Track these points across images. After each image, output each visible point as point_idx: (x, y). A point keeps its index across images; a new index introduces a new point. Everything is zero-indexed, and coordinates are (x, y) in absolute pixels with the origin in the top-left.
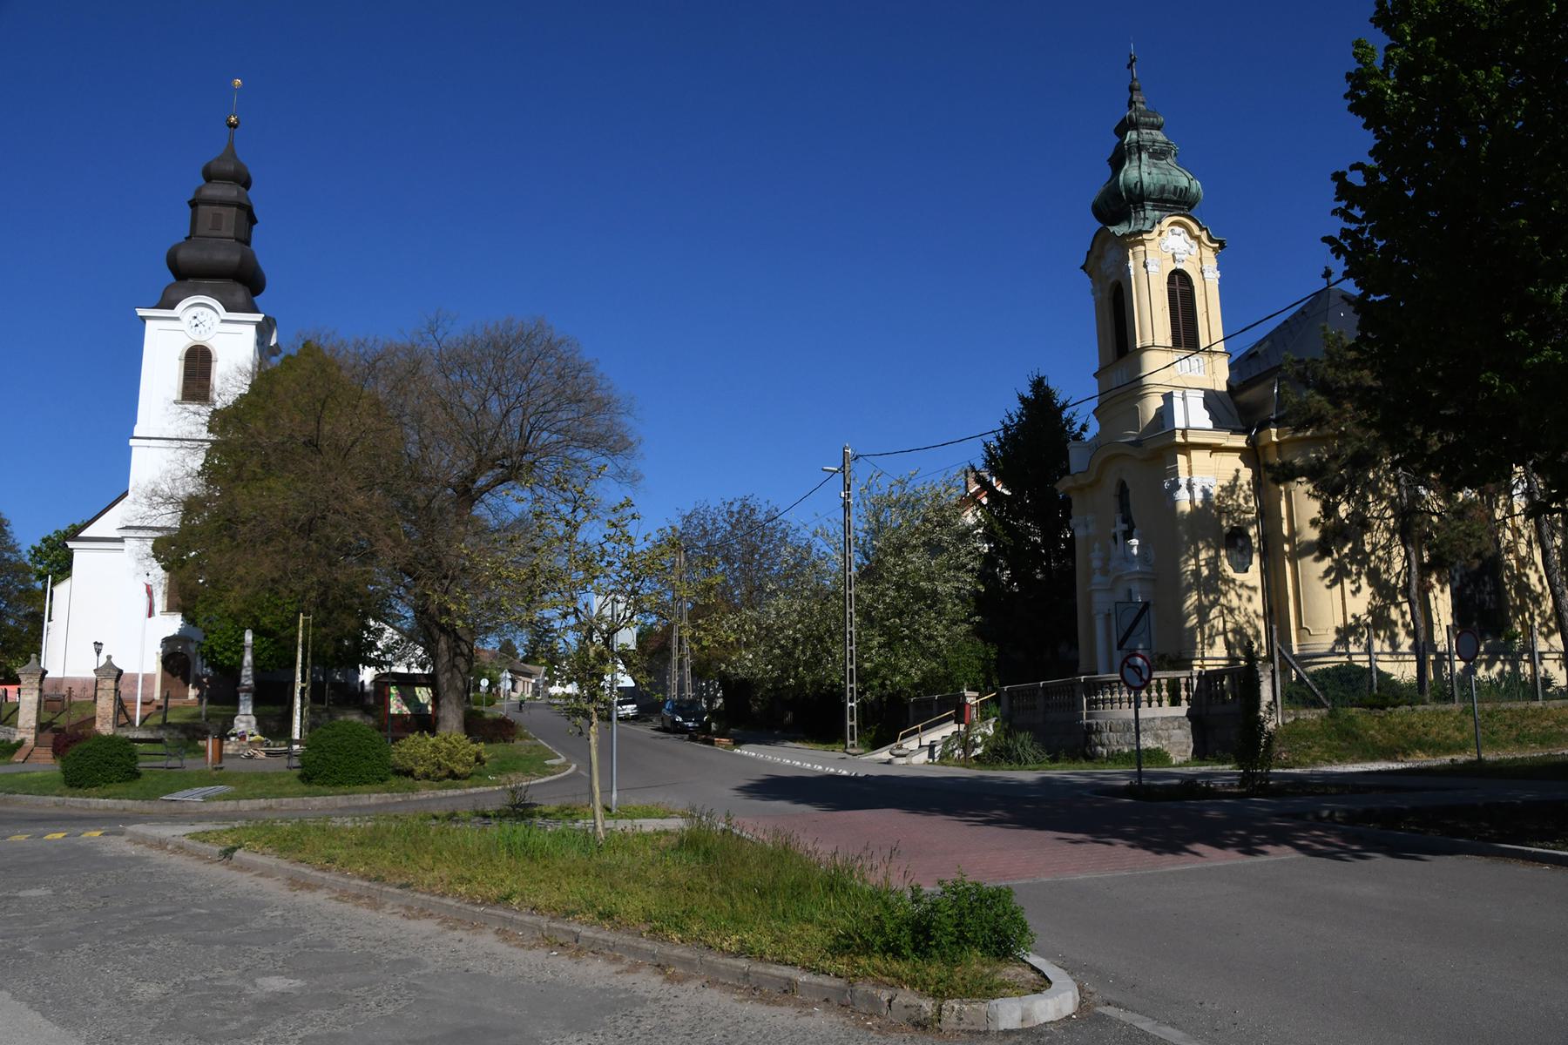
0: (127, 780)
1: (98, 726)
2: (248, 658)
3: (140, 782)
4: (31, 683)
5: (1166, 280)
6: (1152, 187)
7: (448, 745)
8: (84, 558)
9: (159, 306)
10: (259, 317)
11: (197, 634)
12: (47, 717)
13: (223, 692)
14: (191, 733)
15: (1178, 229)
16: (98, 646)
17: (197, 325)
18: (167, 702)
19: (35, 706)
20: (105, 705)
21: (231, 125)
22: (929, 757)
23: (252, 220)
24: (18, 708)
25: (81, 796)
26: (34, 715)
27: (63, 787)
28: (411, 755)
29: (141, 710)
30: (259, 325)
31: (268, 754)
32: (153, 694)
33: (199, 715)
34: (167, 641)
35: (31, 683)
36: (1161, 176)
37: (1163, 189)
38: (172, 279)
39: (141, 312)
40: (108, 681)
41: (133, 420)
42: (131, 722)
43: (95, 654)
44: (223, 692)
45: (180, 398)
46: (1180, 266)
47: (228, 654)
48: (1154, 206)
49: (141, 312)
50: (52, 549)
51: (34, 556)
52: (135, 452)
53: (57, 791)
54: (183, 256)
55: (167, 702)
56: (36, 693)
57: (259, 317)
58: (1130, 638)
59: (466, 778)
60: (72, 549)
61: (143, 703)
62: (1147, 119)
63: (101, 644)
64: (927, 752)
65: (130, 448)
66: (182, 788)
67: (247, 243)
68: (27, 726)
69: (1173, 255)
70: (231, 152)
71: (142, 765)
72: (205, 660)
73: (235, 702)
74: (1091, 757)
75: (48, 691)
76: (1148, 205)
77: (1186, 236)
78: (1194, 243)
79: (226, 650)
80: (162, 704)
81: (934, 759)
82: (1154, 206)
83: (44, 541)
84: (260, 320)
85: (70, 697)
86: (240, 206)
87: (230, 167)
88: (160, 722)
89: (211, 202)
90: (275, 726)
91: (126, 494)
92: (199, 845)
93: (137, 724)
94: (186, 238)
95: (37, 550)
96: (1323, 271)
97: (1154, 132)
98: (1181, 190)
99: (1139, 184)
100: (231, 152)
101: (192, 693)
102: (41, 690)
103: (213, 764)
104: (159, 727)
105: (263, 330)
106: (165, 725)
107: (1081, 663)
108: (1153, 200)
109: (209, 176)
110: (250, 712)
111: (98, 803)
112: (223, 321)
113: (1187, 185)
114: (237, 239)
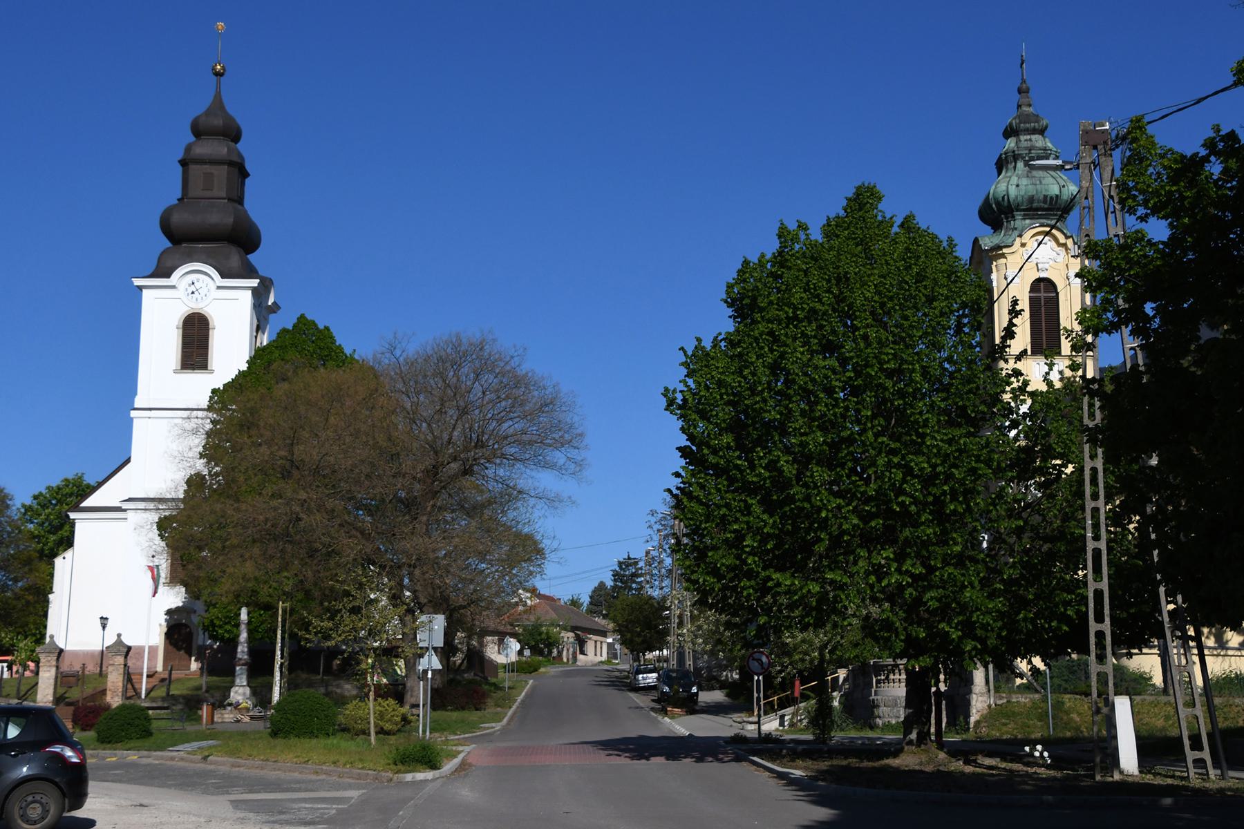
0: (144, 737)
1: (108, 698)
2: (244, 636)
3: (152, 739)
4: (49, 661)
7: (381, 709)
8: (85, 528)
9: (153, 275)
10: (254, 283)
11: (199, 606)
12: (61, 691)
13: (220, 666)
14: (191, 703)
16: (104, 621)
17: (193, 293)
18: (170, 674)
19: (52, 681)
20: (115, 679)
21: (219, 74)
22: (780, 725)
23: (244, 174)
24: (37, 683)
25: (110, 749)
26: (51, 691)
27: (96, 743)
28: (352, 716)
29: (147, 682)
30: (255, 291)
31: (252, 718)
32: (156, 667)
33: (199, 688)
34: (169, 612)
35: (49, 661)
37: (1031, 199)
38: (168, 244)
39: (138, 282)
40: (119, 657)
41: (133, 391)
42: (138, 694)
43: (101, 628)
44: (220, 666)
45: (179, 368)
46: (1043, 275)
47: (228, 627)
48: (1024, 215)
49: (138, 282)
50: (44, 507)
51: (25, 514)
52: (136, 423)
53: (92, 747)
54: (176, 219)
55: (170, 674)
56: (53, 670)
57: (254, 283)
59: (394, 734)
60: (74, 519)
61: (148, 676)
62: (1028, 125)
63: (107, 619)
64: (778, 721)
65: (132, 419)
66: (183, 743)
67: (240, 200)
68: (45, 700)
69: (1037, 264)
70: (218, 105)
71: (155, 725)
72: (206, 634)
73: (231, 673)
74: (872, 727)
75: (65, 667)
76: (1018, 215)
77: (1053, 244)
78: (1062, 251)
79: (226, 624)
80: (166, 676)
81: (784, 726)
82: (1024, 215)
83: (35, 497)
84: (256, 285)
85: (83, 672)
86: (231, 164)
87: (218, 122)
88: (164, 694)
89: (201, 161)
90: (261, 694)
91: (128, 461)
92: (192, 757)
93: (143, 696)
94: (179, 200)
95: (28, 509)
97: (1034, 137)
99: (1006, 197)
100: (218, 105)
101: (194, 666)
102: (57, 667)
103: (207, 725)
104: (163, 699)
105: (259, 295)
106: (169, 697)
108: (1023, 210)
109: (199, 131)
110: (245, 684)
111: (123, 754)
112: (219, 288)
113: (1058, 193)
114: (229, 199)
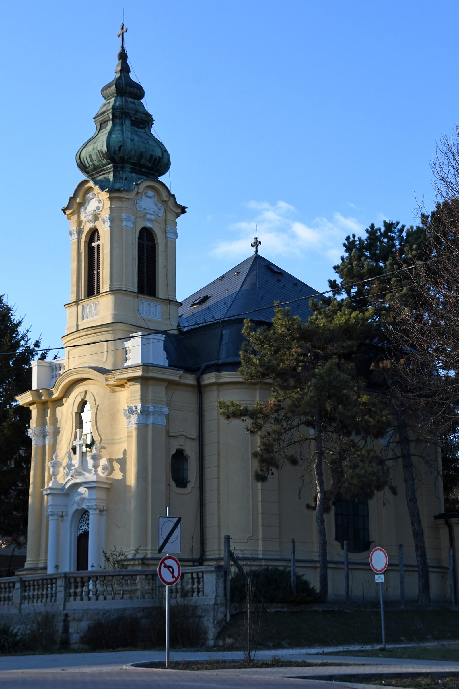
5: (137, 235)
6: (133, 153)
15: (151, 193)
36: (141, 144)
37: (141, 155)
58: (167, 544)
96: (252, 241)
98: (155, 159)
107: (27, 559)
